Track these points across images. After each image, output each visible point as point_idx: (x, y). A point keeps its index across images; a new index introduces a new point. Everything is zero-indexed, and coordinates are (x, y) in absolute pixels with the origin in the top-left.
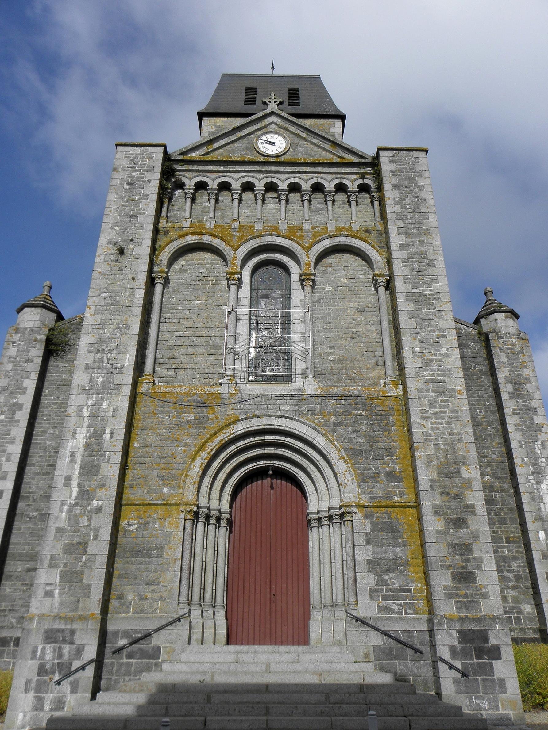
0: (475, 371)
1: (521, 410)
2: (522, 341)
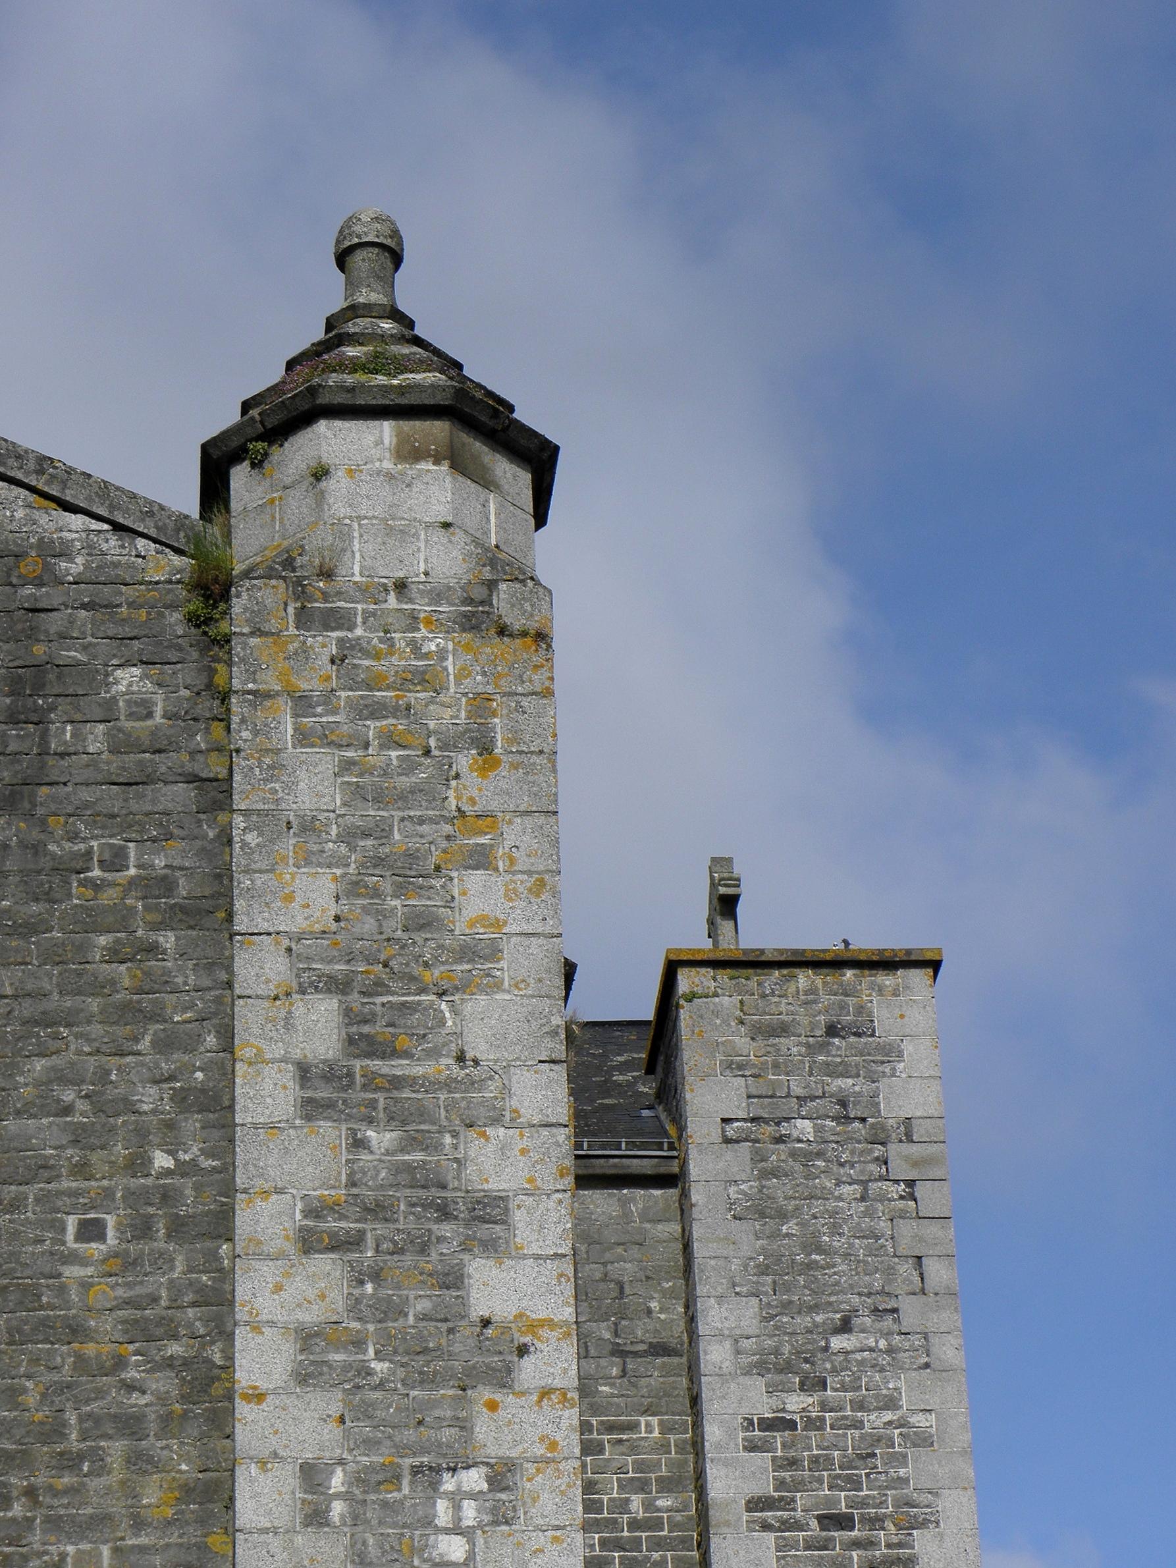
0: (109, 897)
1: (378, 1210)
2: (495, 648)
